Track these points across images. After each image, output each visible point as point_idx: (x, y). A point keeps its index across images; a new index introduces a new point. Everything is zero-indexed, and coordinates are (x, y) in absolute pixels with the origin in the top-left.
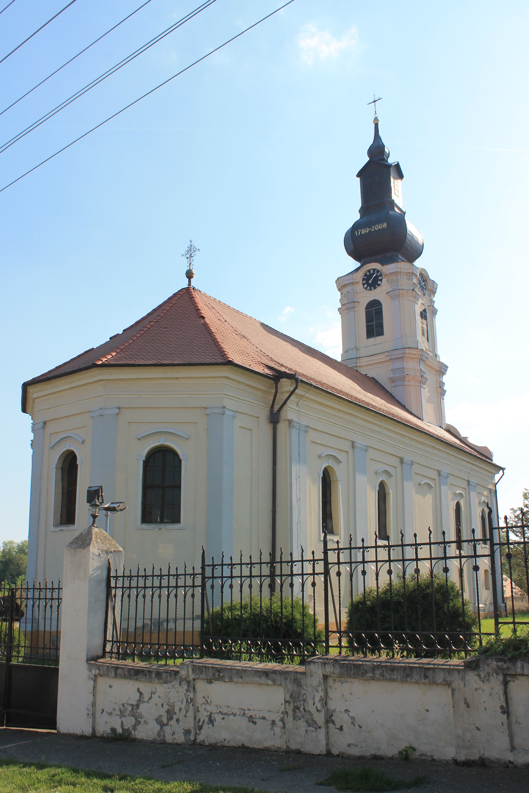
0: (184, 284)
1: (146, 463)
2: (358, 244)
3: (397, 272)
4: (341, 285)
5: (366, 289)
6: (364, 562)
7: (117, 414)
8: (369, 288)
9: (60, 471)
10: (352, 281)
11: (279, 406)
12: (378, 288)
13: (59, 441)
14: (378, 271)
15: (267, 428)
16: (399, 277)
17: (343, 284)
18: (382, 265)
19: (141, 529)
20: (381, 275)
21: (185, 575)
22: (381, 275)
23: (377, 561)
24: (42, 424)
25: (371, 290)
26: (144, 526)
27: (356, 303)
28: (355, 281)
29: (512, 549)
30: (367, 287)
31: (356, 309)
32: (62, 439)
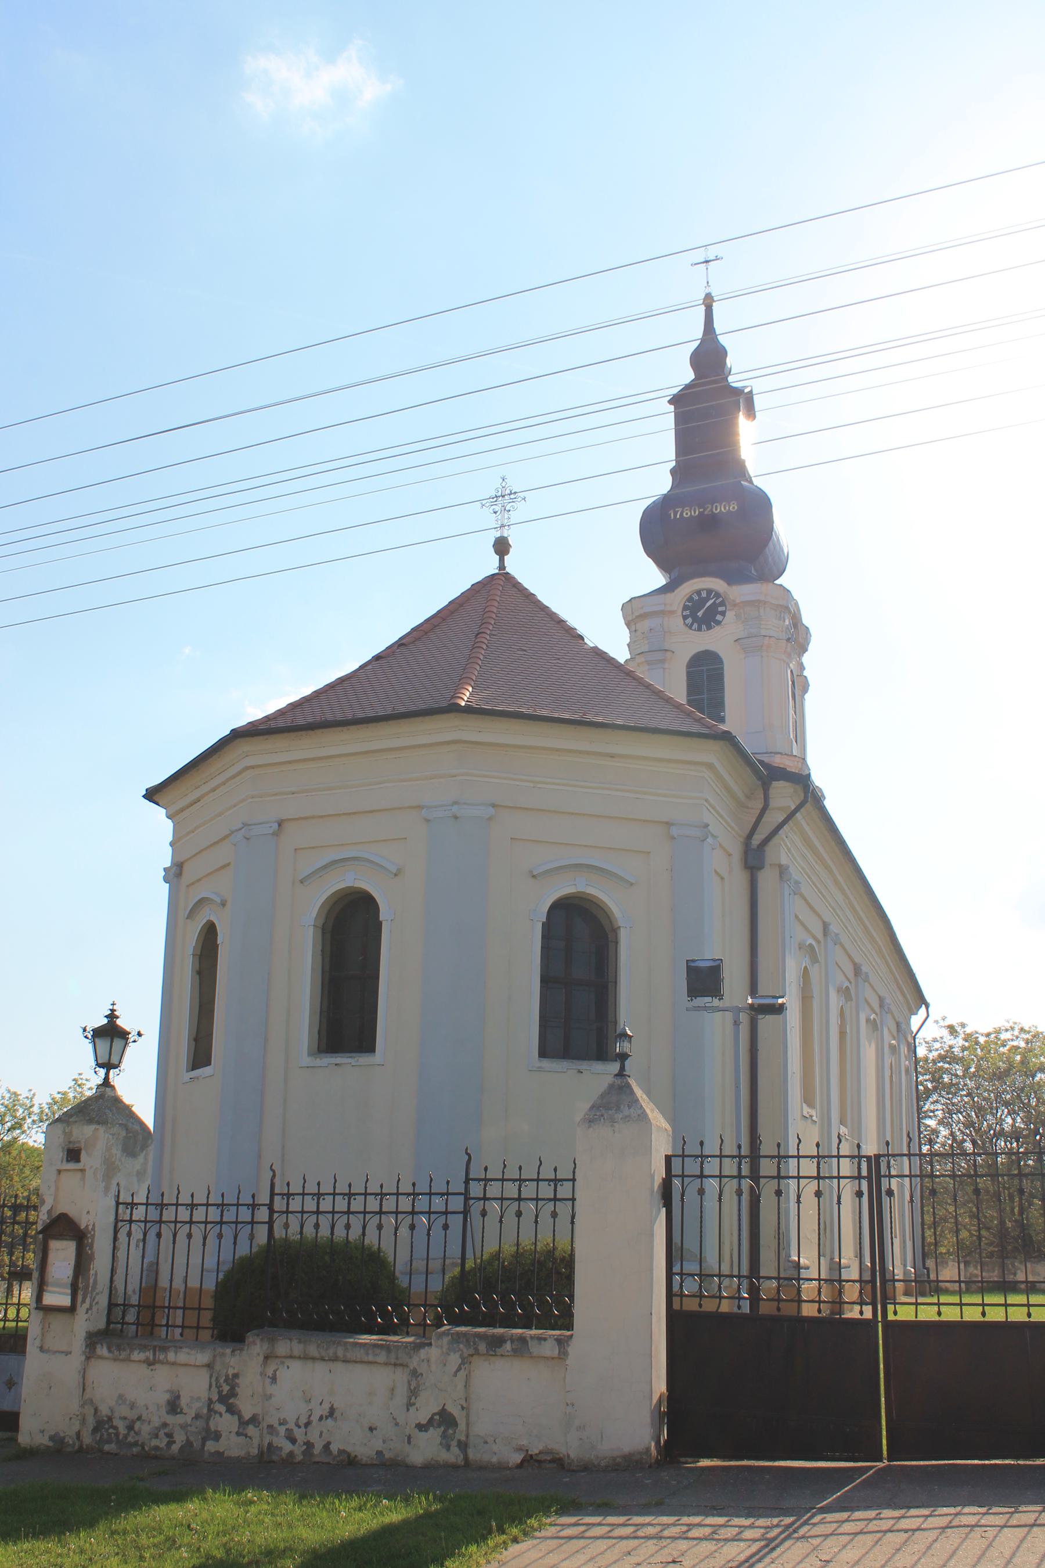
0: (490, 566)
3: (759, 601)
4: (637, 614)
5: (690, 627)
6: (702, 1176)
7: (490, 819)
8: (695, 626)
9: (320, 932)
10: (661, 608)
11: (764, 837)
13: (325, 867)
14: (718, 595)
15: (739, 879)
16: (762, 611)
17: (641, 612)
18: (729, 584)
19: (540, 1070)
20: (722, 604)
21: (207, 1205)
22: (722, 604)
23: (721, 1177)
24: (276, 826)
25: (699, 629)
26: (546, 1064)
27: (669, 654)
28: (668, 608)
30: (692, 625)
31: (666, 666)
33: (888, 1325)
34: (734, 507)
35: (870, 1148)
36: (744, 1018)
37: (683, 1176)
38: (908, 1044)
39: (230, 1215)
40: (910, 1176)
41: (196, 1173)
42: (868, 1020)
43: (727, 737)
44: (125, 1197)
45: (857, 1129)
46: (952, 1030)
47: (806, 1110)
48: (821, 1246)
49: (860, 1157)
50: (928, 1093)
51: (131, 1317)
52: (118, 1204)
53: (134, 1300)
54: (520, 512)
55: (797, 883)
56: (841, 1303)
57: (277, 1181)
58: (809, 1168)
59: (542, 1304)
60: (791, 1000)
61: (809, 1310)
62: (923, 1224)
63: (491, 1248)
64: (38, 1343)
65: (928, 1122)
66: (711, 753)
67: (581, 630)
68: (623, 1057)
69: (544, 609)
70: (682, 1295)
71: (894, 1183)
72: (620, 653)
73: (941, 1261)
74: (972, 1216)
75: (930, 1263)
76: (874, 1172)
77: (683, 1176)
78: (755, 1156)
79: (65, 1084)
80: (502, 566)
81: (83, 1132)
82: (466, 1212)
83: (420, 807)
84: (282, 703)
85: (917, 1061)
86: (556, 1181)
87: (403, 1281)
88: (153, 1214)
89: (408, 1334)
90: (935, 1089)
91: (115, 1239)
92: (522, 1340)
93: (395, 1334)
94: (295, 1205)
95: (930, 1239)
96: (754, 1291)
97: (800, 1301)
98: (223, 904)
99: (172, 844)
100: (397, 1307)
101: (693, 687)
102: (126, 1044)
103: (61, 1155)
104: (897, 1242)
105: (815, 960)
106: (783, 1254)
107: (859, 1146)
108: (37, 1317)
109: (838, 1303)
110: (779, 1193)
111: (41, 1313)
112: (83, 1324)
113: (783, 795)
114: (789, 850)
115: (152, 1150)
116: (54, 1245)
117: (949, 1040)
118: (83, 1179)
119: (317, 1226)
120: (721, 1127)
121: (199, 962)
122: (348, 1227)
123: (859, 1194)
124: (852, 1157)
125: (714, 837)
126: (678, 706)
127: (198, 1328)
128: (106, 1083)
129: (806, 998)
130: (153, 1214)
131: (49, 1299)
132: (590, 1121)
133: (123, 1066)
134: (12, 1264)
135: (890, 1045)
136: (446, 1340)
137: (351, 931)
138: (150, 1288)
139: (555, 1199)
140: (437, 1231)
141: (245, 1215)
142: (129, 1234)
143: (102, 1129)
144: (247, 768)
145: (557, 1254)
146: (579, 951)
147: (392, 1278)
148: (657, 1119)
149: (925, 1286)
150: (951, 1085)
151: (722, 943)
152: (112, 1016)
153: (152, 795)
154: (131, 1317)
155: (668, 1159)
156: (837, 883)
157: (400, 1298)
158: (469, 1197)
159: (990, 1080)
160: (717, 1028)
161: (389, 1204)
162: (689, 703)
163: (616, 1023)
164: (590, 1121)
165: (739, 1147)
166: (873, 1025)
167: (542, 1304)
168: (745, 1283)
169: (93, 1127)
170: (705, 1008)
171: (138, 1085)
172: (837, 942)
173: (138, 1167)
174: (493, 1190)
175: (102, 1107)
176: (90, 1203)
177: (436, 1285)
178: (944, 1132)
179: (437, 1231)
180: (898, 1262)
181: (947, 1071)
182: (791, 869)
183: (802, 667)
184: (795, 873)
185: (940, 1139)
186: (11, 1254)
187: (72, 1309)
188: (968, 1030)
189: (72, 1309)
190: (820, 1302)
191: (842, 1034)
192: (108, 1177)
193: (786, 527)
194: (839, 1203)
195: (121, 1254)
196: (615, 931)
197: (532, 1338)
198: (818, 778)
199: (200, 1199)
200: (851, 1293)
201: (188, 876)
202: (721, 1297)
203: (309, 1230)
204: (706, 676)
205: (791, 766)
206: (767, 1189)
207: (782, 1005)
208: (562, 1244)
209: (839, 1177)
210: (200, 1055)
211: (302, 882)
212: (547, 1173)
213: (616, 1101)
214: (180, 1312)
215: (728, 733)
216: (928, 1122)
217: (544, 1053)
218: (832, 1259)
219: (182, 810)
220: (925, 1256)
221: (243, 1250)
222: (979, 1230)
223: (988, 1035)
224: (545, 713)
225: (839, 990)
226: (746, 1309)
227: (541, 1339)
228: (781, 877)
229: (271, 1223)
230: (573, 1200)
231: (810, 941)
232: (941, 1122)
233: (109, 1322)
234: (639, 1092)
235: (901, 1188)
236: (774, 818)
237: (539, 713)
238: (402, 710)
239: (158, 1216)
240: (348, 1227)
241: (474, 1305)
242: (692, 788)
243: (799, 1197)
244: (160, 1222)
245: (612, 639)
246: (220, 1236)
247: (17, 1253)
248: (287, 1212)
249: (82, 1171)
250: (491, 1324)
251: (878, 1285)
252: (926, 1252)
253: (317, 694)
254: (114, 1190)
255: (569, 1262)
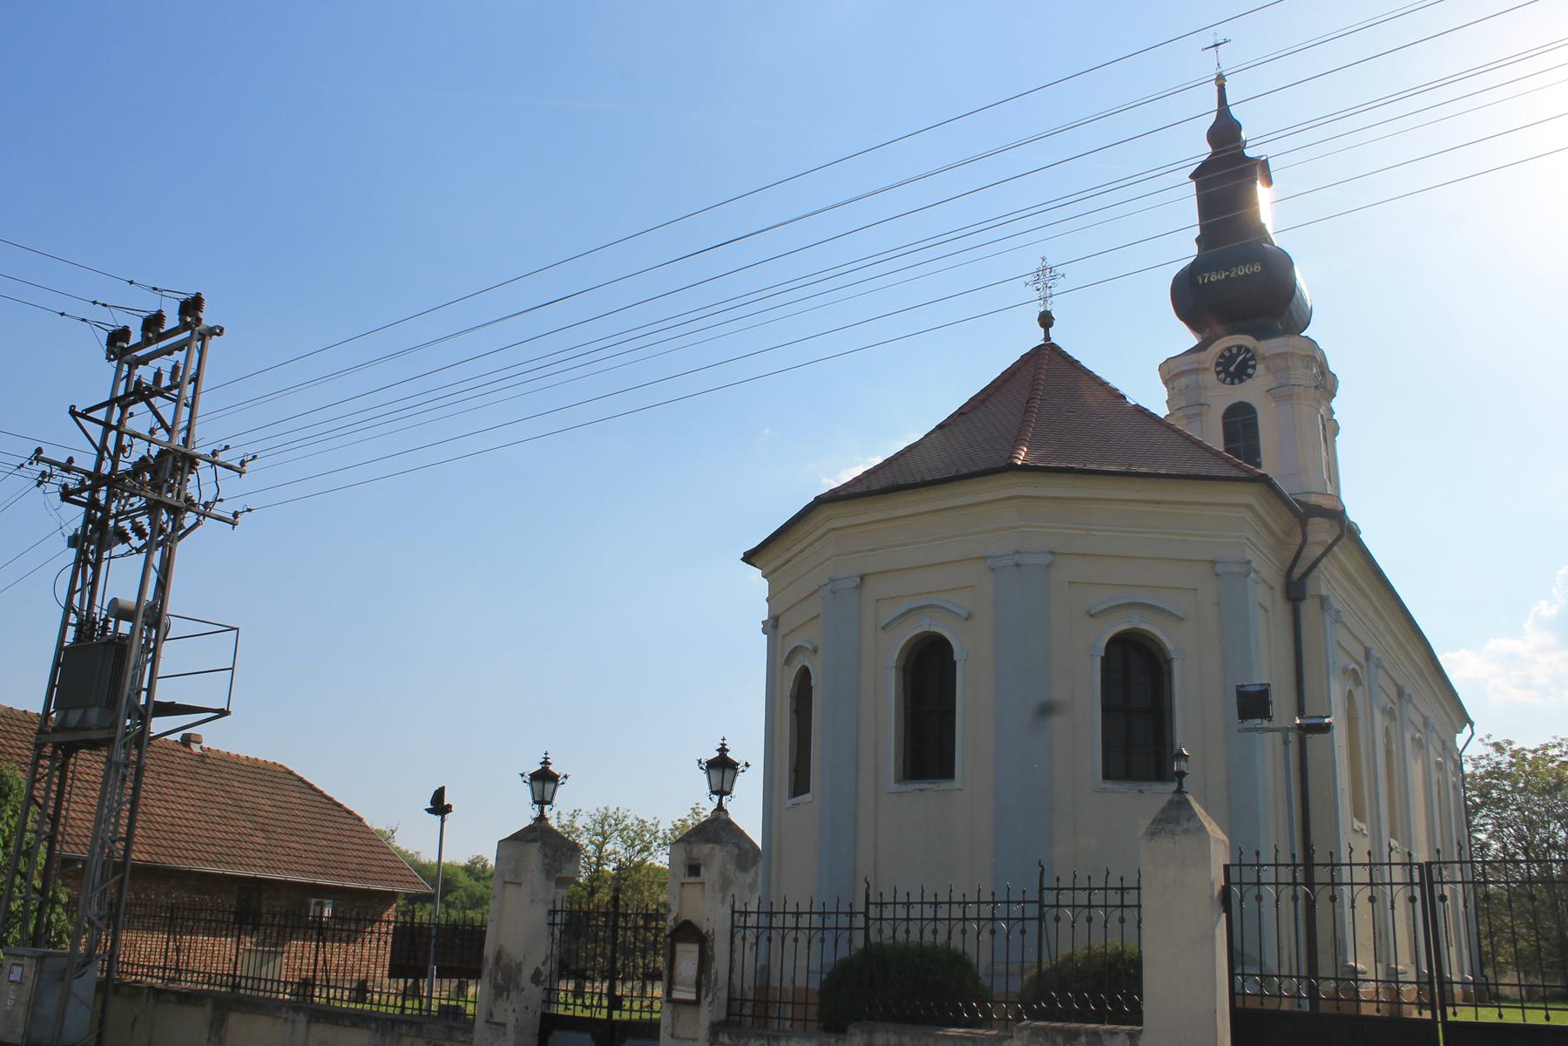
0: (1036, 338)
1: (1106, 661)
2: (1193, 296)
5: (1224, 381)
6: (1259, 883)
7: (1049, 566)
12: (1249, 381)
13: (903, 615)
14: (1248, 350)
15: (1282, 611)
21: (811, 913)
22: (1253, 358)
25: (1232, 383)
26: (1109, 785)
29: (603, 955)
32: (910, 611)
33: (1449, 1026)
34: (1257, 268)
35: (1421, 856)
36: (1292, 737)
37: (1241, 884)
38: (1455, 761)
39: (831, 922)
40: (1463, 882)
41: (800, 886)
42: (1413, 739)
43: (1265, 480)
44: (739, 906)
45: (1408, 840)
46: (1498, 747)
47: (1357, 824)
48: (1378, 948)
49: (1411, 864)
50: (1478, 807)
51: (747, 1010)
52: (733, 912)
53: (750, 995)
54: (1060, 285)
55: (1338, 612)
56: (1400, 1003)
57: (871, 891)
58: (1362, 875)
59: (1113, 1001)
60: (1336, 719)
61: (1367, 1010)
62: (1479, 933)
63: (1065, 950)
64: (669, 1030)
65: (1479, 836)
66: (1247, 495)
67: (1123, 391)
68: (1181, 775)
69: (1088, 373)
70: (1244, 994)
71: (1447, 889)
72: (1162, 411)
73: (1499, 970)
74: (1529, 927)
75: (1489, 972)
76: (1426, 879)
77: (1241, 884)
78: (1309, 865)
79: (684, 813)
80: (1047, 338)
81: (703, 850)
82: (1041, 918)
83: (986, 558)
84: (858, 471)
85: (1464, 777)
86: (1122, 890)
87: (986, 982)
88: (764, 921)
89: (991, 1028)
90: (1483, 804)
91: (732, 943)
92: (1096, 1033)
93: (980, 1027)
94: (888, 912)
95: (1486, 948)
96: (1313, 992)
97: (1358, 1001)
98: (815, 651)
99: (768, 600)
100: (982, 1003)
101: (1229, 437)
102: (736, 774)
103: (683, 870)
104: (1453, 950)
105: (1358, 682)
106: (1340, 960)
107: (1410, 855)
108: (668, 1009)
109: (1396, 1000)
110: (1333, 899)
111: (671, 1006)
112: (707, 1014)
113: (1320, 531)
114: (1329, 581)
115: (761, 863)
116: (680, 947)
117: (1496, 757)
118: (703, 891)
119: (907, 931)
120: (1275, 836)
121: (796, 704)
122: (935, 932)
123: (1412, 899)
124: (1404, 864)
125: (1257, 572)
126: (1217, 454)
127: (806, 1020)
128: (720, 807)
129: (1352, 720)
130: (764, 921)
131: (676, 995)
132: (1152, 834)
133: (734, 793)
134: (645, 966)
135: (1437, 763)
136: (1026, 1033)
137: (928, 671)
138: (763, 987)
139: (1122, 906)
140: (1015, 936)
141: (844, 921)
142: (744, 939)
143: (718, 847)
144: (830, 531)
145: (1126, 956)
146: (1136, 675)
147: (976, 978)
148: (1214, 831)
149: (1484, 994)
150: (1500, 800)
151: (1267, 667)
152: (723, 750)
153: (749, 558)
154: (747, 1010)
155: (1226, 868)
156: (1377, 611)
157: (983, 996)
158: (1043, 903)
159: (1539, 794)
160: (1268, 750)
161: (972, 911)
162: (1227, 450)
163: (1172, 746)
164: (1152, 834)
165: (1293, 856)
166: (1418, 743)
167: (1113, 1001)
168: (1304, 983)
169: (710, 846)
170: (1256, 730)
171: (747, 809)
172: (1379, 666)
173: (749, 880)
174: (1066, 898)
175: (718, 829)
176: (711, 913)
177: (1016, 986)
178: (1495, 845)
179: (1015, 936)
180: (1455, 969)
181: (1495, 787)
182: (1332, 599)
183: (1331, 412)
184: (1335, 603)
185: (1492, 852)
186: (644, 958)
187: (697, 1003)
188: (1515, 747)
189: (697, 1003)
190: (1378, 1002)
191: (1389, 752)
192: (724, 889)
193: (1304, 280)
194: (1393, 908)
195: (738, 956)
196: (1169, 662)
197: (1105, 1032)
198: (1353, 515)
199: (804, 907)
200: (1409, 992)
201: (784, 627)
202: (1281, 996)
203: (901, 936)
204: (1240, 422)
205: (1326, 503)
206: (1322, 895)
207: (1329, 724)
208: (1131, 946)
209: (1391, 884)
210: (800, 783)
211: (883, 629)
212: (1114, 882)
213: (1176, 815)
214: (789, 1007)
215: (1265, 475)
216: (1479, 836)
217: (1107, 776)
218: (1388, 965)
219: (775, 570)
220: (1482, 966)
221: (843, 953)
222: (1538, 940)
223: (1535, 751)
224: (1094, 467)
225: (1383, 711)
226: (1306, 1006)
227: (1113, 1033)
228: (1322, 607)
229: (867, 929)
230: (1139, 906)
231: (1353, 666)
232: (1491, 836)
233: (729, 1014)
234: (1197, 807)
235: (1455, 899)
236: (1313, 552)
237: (1089, 467)
238: (965, 471)
239: (769, 923)
240: (935, 932)
241: (1051, 1001)
242: (1230, 525)
243: (1353, 902)
244: (770, 928)
245: (1153, 397)
246: (823, 940)
247: (650, 957)
248: (881, 919)
249: (702, 884)
250: (1068, 1020)
251: (1436, 989)
252: (1482, 960)
253: (888, 462)
254: (729, 898)
255: (1137, 963)
